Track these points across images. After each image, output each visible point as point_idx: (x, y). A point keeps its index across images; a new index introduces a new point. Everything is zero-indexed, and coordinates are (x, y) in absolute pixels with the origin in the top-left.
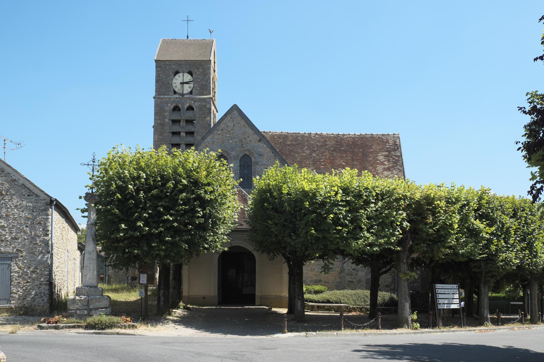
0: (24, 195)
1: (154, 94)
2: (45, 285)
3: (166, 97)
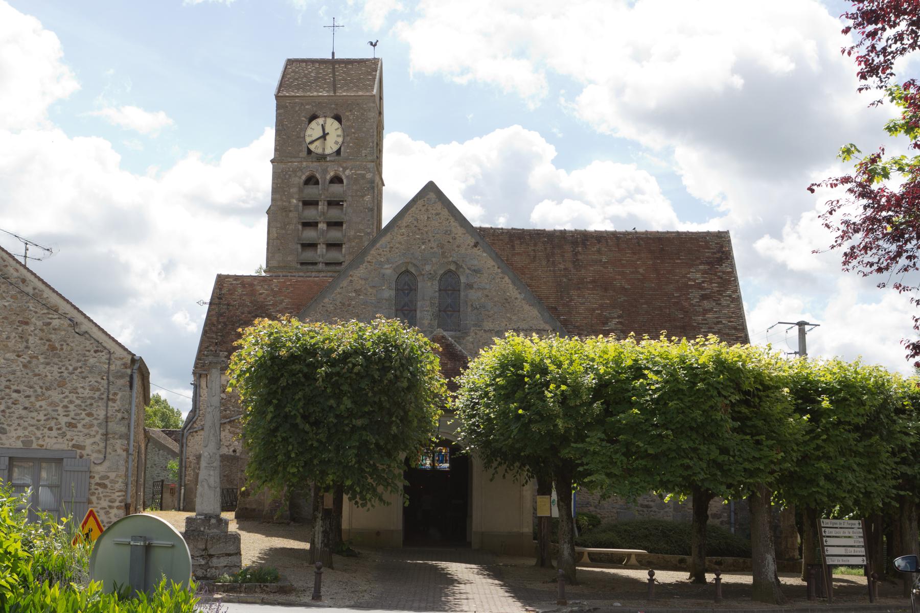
0: (89, 351)
2: (118, 508)
3: (294, 160)
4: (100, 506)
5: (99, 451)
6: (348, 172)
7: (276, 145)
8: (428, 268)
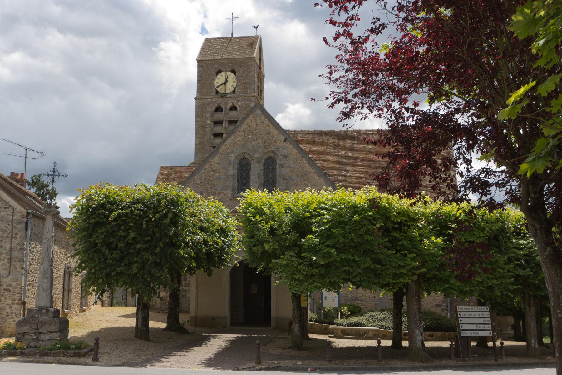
1: (195, 95)
2: (17, 304)
3: (208, 97)
4: (6, 303)
5: (6, 269)
6: (239, 103)
7: (197, 89)
8: (256, 155)
